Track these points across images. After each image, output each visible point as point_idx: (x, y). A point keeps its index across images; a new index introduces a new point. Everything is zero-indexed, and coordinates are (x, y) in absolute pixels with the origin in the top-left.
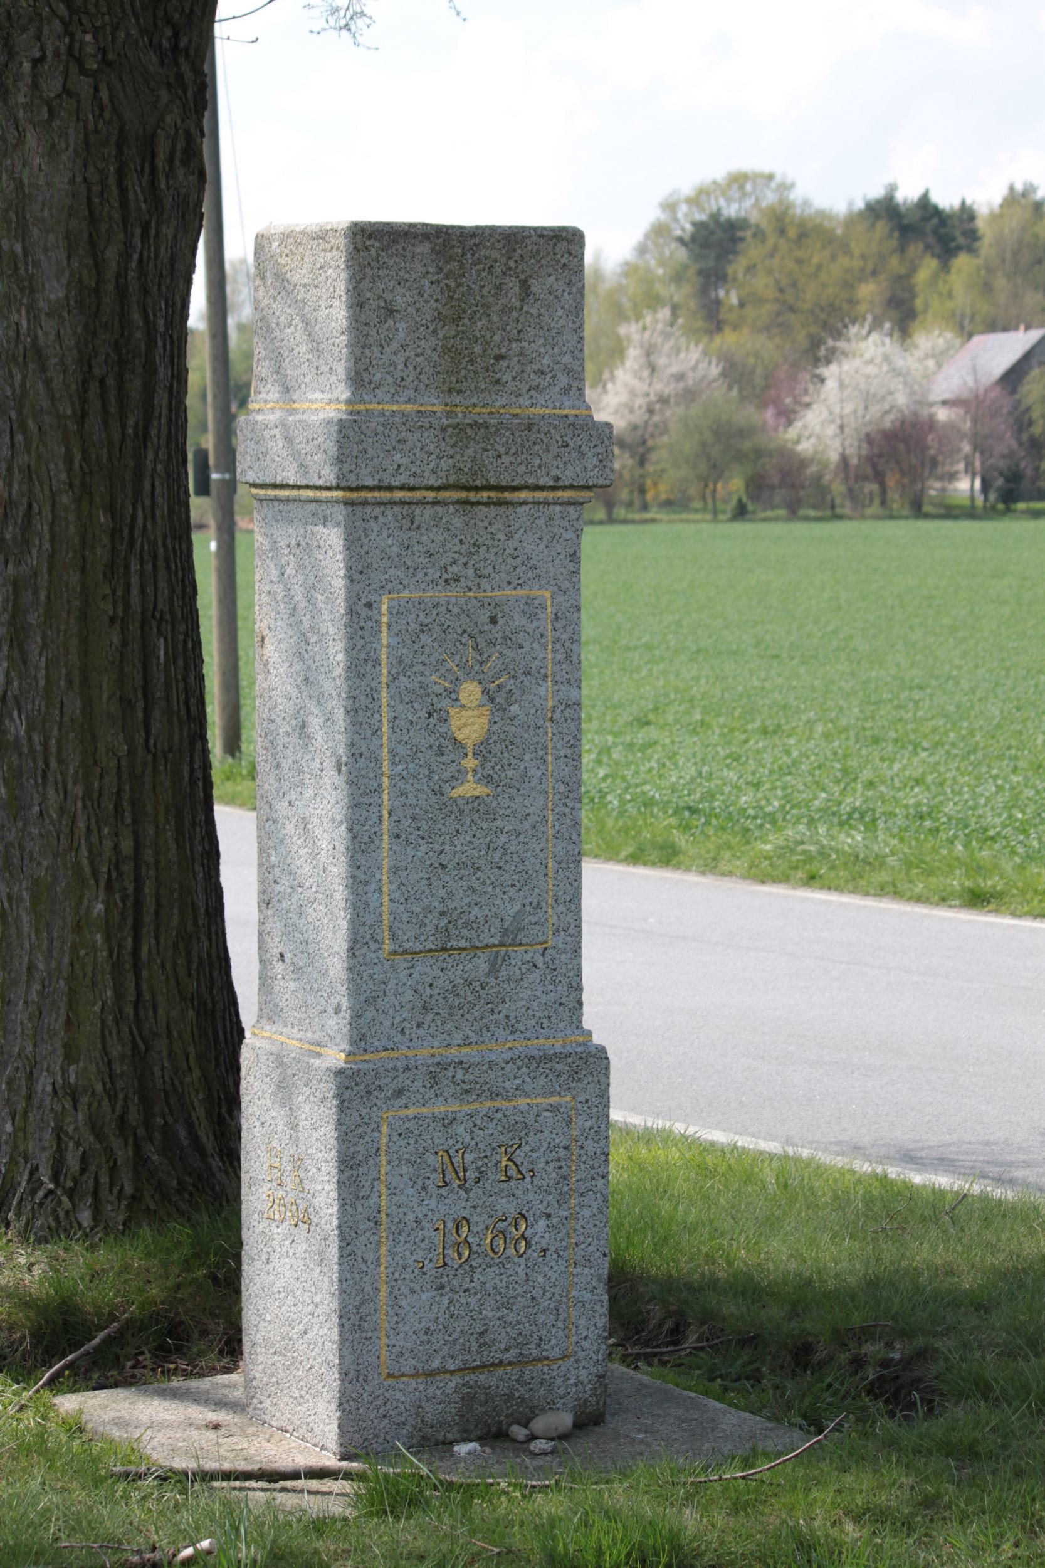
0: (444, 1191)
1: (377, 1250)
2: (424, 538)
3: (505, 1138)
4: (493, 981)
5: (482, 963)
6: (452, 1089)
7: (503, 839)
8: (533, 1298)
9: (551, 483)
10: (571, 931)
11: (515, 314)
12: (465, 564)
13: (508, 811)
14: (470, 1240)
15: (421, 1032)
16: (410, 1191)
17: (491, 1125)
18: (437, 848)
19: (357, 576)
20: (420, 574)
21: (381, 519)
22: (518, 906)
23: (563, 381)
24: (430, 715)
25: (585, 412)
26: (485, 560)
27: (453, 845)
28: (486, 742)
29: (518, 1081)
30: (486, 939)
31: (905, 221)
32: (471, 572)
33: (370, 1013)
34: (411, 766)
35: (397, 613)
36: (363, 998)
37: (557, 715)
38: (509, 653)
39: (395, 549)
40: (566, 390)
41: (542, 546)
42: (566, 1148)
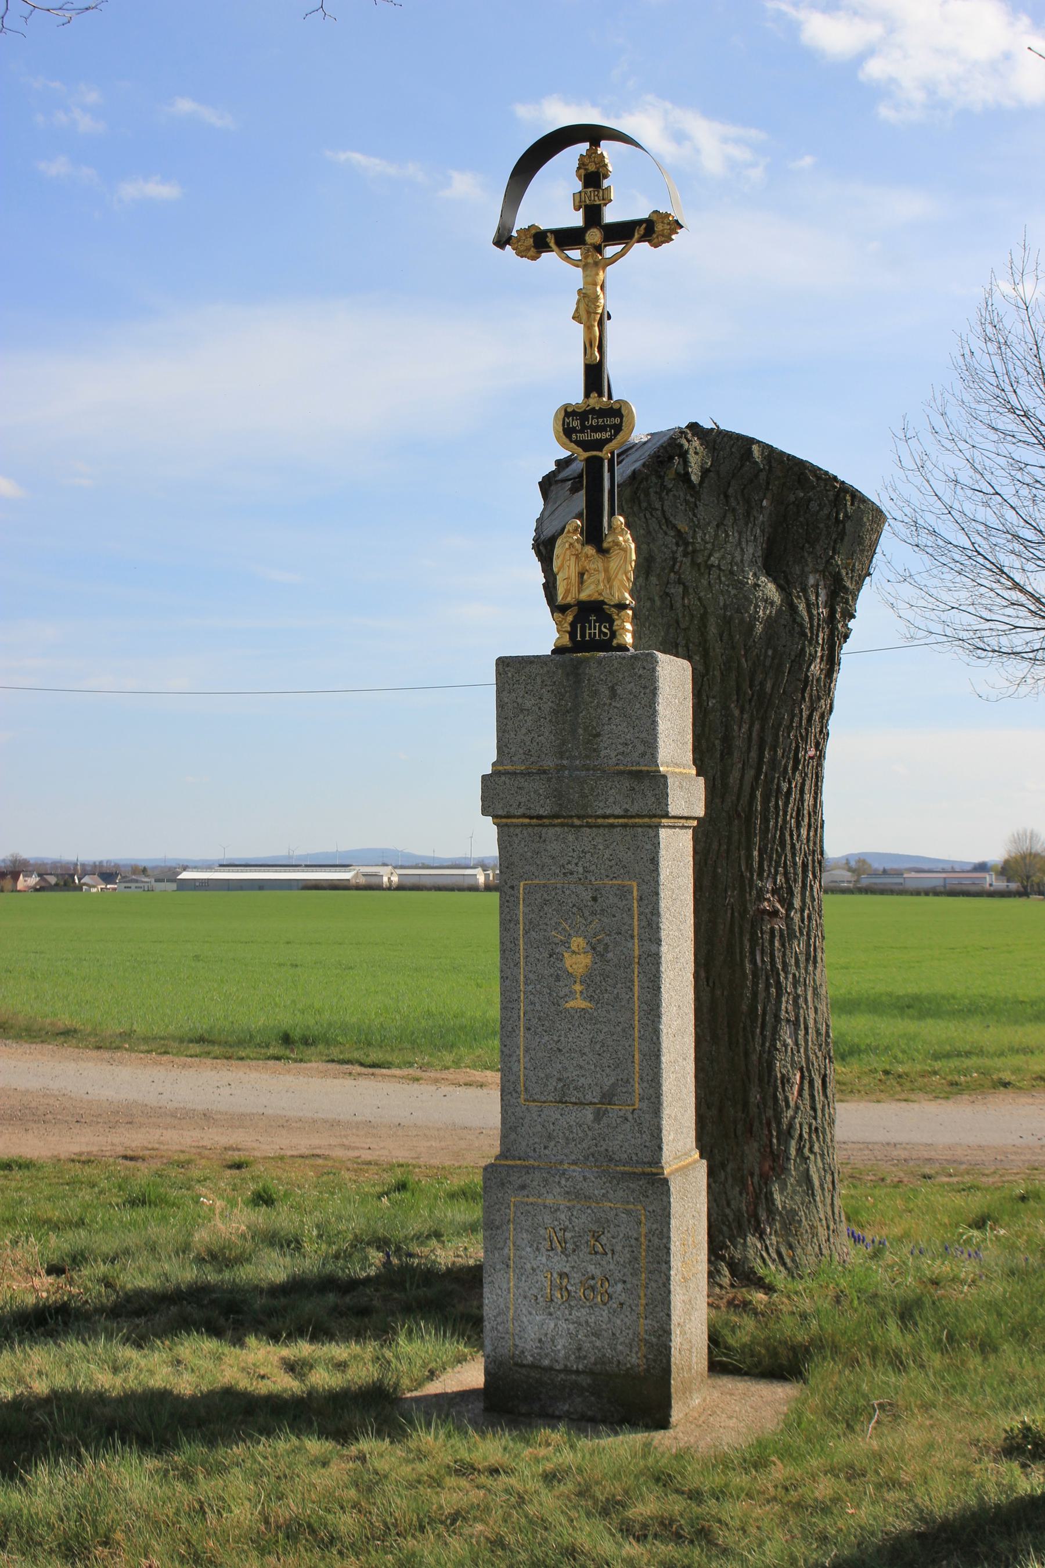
0: (551, 1254)
1: (509, 1283)
2: (548, 848)
3: (594, 1228)
4: (597, 1126)
5: (589, 1114)
6: (559, 1190)
7: (602, 1037)
8: (614, 1334)
9: (622, 813)
10: (652, 1100)
11: (606, 708)
12: (576, 864)
13: (605, 1020)
14: (569, 1288)
15: (547, 1152)
16: (528, 1249)
17: (584, 1217)
18: (556, 1038)
19: (505, 869)
20: (546, 870)
21: (520, 836)
22: (613, 1080)
23: (641, 748)
24: (551, 956)
25: (653, 769)
26: (590, 861)
27: (566, 1036)
28: (590, 976)
29: (604, 1191)
30: (589, 1097)
31: (566, 640)
32: (581, 870)
33: (513, 1136)
34: (538, 986)
35: (528, 892)
36: (508, 1126)
37: (642, 961)
38: (605, 920)
39: (529, 854)
40: (643, 755)
41: (629, 853)
42: (636, 1239)
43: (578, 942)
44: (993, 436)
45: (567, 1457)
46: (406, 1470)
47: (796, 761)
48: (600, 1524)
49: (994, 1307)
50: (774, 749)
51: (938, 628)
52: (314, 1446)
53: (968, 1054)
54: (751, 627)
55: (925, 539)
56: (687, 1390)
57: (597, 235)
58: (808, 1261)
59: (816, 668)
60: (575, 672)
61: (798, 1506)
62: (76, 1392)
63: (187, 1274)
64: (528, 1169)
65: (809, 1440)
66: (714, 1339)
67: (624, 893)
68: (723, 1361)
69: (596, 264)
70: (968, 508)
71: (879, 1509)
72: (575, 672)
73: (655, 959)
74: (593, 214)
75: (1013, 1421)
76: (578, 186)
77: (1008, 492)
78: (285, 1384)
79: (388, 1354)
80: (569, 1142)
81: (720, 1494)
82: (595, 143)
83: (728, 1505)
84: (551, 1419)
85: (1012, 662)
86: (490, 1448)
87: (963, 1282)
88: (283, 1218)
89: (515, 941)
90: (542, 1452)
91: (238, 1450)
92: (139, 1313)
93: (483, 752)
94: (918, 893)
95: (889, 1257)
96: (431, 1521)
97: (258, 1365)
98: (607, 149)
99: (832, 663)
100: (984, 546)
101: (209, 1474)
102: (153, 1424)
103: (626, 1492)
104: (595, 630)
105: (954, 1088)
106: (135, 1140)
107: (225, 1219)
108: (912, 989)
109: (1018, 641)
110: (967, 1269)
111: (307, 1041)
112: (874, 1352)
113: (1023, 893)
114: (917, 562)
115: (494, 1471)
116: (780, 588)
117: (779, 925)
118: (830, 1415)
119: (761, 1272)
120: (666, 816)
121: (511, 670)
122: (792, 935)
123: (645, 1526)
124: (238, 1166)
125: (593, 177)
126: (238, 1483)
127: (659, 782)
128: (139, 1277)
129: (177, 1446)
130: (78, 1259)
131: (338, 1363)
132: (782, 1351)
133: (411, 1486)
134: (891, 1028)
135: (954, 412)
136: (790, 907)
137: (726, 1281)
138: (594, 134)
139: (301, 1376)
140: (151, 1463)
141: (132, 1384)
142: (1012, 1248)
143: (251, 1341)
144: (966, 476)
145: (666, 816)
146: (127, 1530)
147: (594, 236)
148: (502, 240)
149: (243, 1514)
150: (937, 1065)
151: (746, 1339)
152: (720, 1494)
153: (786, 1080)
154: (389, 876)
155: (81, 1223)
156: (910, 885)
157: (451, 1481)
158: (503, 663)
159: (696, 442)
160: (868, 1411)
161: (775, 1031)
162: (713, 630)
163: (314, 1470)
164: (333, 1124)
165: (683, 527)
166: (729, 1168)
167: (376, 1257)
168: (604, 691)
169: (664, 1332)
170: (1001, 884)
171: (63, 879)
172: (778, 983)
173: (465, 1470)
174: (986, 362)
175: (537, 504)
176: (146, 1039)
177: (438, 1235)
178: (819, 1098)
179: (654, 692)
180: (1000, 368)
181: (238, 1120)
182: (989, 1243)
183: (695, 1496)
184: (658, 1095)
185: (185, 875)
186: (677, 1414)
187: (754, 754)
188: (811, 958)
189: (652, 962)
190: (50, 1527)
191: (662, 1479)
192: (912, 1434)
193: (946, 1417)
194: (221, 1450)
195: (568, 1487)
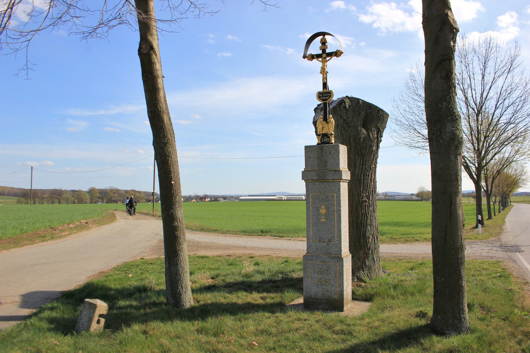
31: (320, 142)
43: (323, 207)
44: (413, 100)
45: (321, 317)
46: (286, 319)
47: (370, 168)
48: (328, 331)
49: (414, 286)
50: (365, 165)
51: (402, 142)
52: (267, 314)
53: (409, 234)
54: (360, 139)
55: (399, 123)
56: (347, 303)
57: (325, 55)
58: (374, 276)
59: (374, 148)
60: (321, 149)
61: (371, 327)
62: (217, 303)
63: (240, 279)
64: (313, 256)
65: (373, 314)
66: (353, 293)
67: (333, 196)
68: (355, 297)
69: (325, 61)
70: (408, 116)
71: (389, 328)
72: (321, 149)
73: (340, 210)
74: (324, 51)
75: (418, 310)
76: (321, 45)
77: (416, 112)
78: (261, 302)
79: (283, 296)
80: (323, 252)
81: (354, 325)
82: (324, 36)
83: (356, 327)
84: (318, 309)
85: (418, 149)
86: (304, 315)
87: (407, 281)
88: (261, 268)
89: (309, 207)
90: (316, 316)
91: (251, 315)
92: (230, 287)
93: (303, 167)
94: (398, 200)
95: (391, 276)
96: (292, 330)
97: (255, 298)
98: (326, 37)
99: (378, 147)
100: (412, 124)
101: (244, 320)
102: (233, 310)
103: (334, 324)
104: (326, 140)
105: (406, 241)
106: (230, 252)
107: (249, 268)
108: (397, 221)
109: (419, 145)
110: (409, 278)
111: (266, 232)
112: (388, 296)
113: (421, 200)
114: (397, 128)
115: (305, 320)
116: (366, 131)
117: (367, 204)
118: (378, 309)
119: (363, 279)
120: (342, 179)
121: (308, 149)
122: (370, 206)
123: (338, 331)
124: (252, 258)
125: (324, 43)
126: (251, 322)
127: (340, 172)
128: (230, 280)
129: (238, 314)
130: (217, 276)
131: (272, 298)
132: (368, 295)
133: (288, 323)
134: (392, 229)
135: (404, 95)
136: (369, 200)
137: (356, 281)
138: (324, 34)
139: (264, 300)
140: (232, 317)
141: (228, 301)
142: (419, 274)
143: (254, 293)
144: (407, 109)
145: (342, 179)
146: (227, 331)
147: (324, 55)
148: (304, 57)
149: (252, 328)
150: (403, 236)
151: (360, 293)
152: (354, 325)
153: (369, 237)
154: (284, 198)
155: (218, 269)
156: (397, 199)
157: (296, 322)
158: (306, 147)
159: (347, 100)
160: (386, 308)
161: (366, 227)
162: (352, 140)
163: (267, 320)
164: (272, 249)
165: (345, 118)
166: (357, 256)
167: (280, 276)
168: (328, 152)
169: (342, 291)
170: (417, 198)
171: (215, 199)
172: (367, 217)
173: (299, 320)
174: (411, 84)
175: (313, 114)
176: (232, 232)
177: (294, 271)
178: (376, 241)
179: (339, 153)
180: (414, 86)
181: (252, 248)
182: (414, 274)
183: (349, 325)
184: (341, 240)
185: (241, 198)
186: (345, 309)
187: (361, 167)
188: (374, 211)
189: (339, 211)
190: (211, 330)
191: (342, 322)
192: (396, 312)
193: (403, 309)
194: (247, 315)
195: (321, 323)
